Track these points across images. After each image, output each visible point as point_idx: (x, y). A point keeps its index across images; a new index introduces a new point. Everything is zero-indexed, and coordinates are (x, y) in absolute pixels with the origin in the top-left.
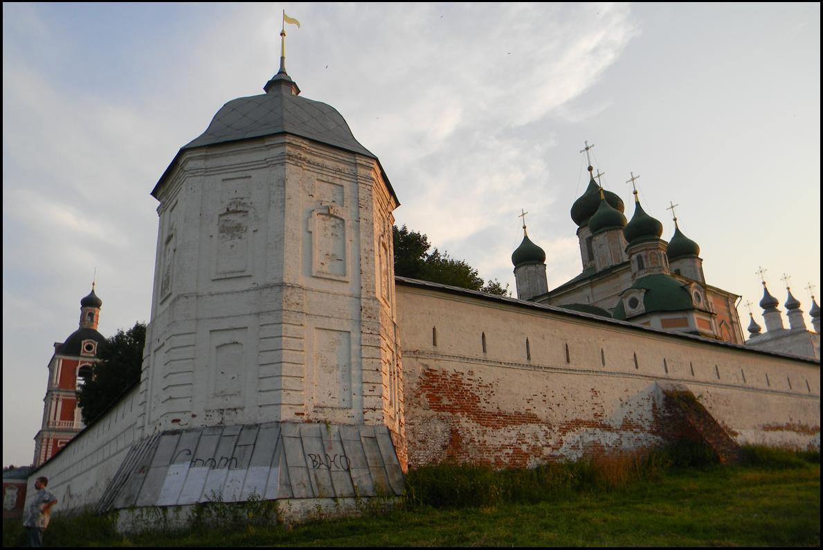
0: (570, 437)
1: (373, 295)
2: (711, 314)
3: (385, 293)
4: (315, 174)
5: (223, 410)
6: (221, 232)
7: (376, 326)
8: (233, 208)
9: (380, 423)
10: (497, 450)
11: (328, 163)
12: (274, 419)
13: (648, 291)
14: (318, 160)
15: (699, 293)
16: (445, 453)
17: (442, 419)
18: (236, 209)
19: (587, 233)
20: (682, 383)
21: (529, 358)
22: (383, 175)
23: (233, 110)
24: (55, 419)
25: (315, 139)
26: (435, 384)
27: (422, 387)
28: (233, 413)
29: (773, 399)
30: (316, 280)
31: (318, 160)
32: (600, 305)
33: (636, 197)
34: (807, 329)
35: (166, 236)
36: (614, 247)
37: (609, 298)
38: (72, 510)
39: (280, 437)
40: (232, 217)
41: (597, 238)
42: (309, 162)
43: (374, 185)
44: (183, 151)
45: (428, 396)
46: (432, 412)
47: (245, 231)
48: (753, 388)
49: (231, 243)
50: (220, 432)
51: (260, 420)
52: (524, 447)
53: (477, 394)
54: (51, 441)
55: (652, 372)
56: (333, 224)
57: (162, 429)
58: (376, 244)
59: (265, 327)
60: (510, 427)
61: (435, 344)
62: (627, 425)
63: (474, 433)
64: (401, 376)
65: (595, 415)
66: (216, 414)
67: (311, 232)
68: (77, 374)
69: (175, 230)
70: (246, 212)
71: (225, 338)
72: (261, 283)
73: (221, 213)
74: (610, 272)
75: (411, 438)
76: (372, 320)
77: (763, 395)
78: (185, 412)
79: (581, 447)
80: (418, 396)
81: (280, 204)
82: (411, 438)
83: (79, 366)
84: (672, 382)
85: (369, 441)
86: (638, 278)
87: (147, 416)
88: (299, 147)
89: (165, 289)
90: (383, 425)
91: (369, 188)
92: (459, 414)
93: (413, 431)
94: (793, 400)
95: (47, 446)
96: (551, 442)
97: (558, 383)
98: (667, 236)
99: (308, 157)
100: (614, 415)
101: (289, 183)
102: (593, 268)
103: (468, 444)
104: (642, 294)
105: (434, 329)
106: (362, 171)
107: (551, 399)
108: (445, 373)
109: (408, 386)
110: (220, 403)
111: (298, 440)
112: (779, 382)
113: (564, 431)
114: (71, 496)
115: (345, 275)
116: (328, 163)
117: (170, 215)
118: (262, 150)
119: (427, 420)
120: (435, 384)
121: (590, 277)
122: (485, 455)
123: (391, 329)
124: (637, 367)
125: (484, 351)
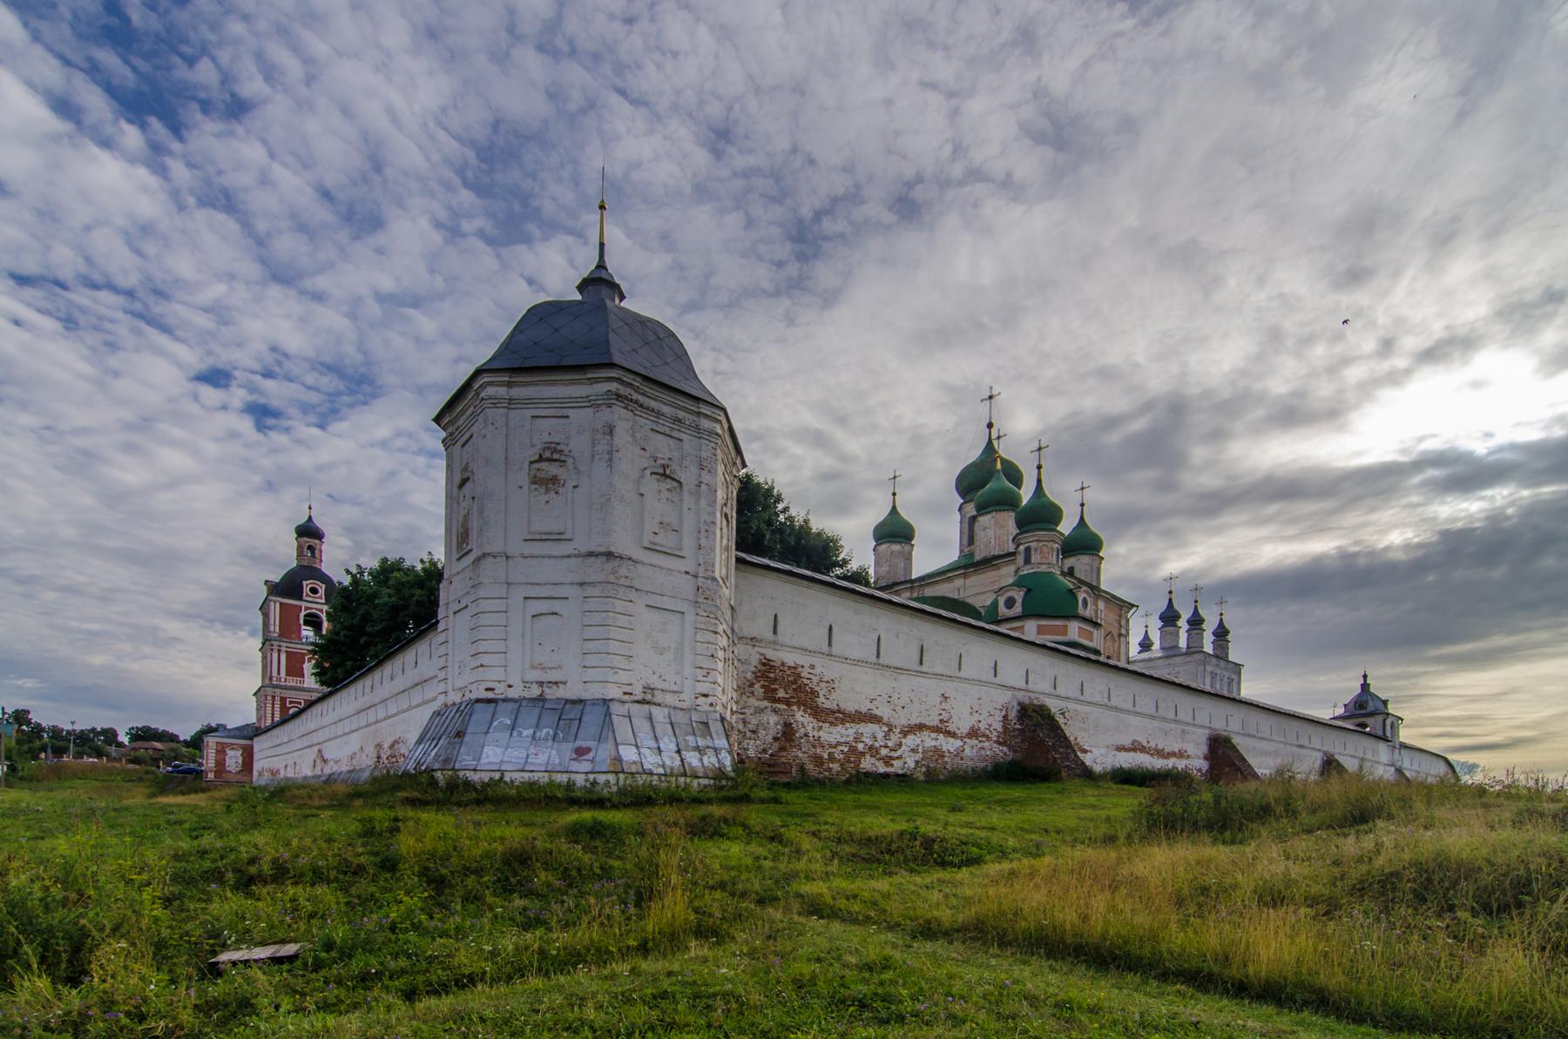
0: (911, 740)
1: (711, 574)
2: (1096, 625)
3: (724, 572)
4: (647, 422)
5: (543, 683)
6: (534, 483)
7: (714, 609)
8: (547, 454)
9: (712, 709)
10: (831, 746)
11: (666, 409)
12: (601, 696)
13: (1029, 590)
14: (653, 404)
15: (1088, 599)
16: (776, 745)
17: (775, 711)
18: (552, 454)
19: (971, 509)
20: (1041, 696)
21: (878, 656)
22: (731, 429)
23: (541, 319)
24: (279, 673)
25: (652, 376)
26: (772, 675)
27: (758, 677)
28: (555, 686)
29: (1134, 720)
30: (647, 552)
31: (653, 404)
32: (971, 601)
33: (1039, 474)
34: (1205, 650)
35: (458, 479)
36: (998, 530)
37: (984, 593)
38: (330, 775)
39: (608, 714)
40: (544, 465)
41: (981, 519)
42: (641, 406)
43: (719, 442)
44: (479, 372)
45: (763, 687)
46: (765, 703)
47: (563, 485)
48: (1116, 708)
49: (546, 498)
50: (541, 704)
51: (585, 696)
52: (860, 747)
53: (816, 689)
54: (278, 699)
55: (1011, 682)
56: (669, 486)
57: (474, 696)
58: (718, 515)
59: (590, 599)
60: (847, 725)
61: (775, 632)
62: (973, 733)
63: (809, 728)
64: (736, 664)
65: (941, 721)
66: (535, 686)
67: (642, 495)
68: (302, 622)
69: (472, 472)
70: (565, 461)
71: (543, 606)
72: (583, 550)
73: (533, 459)
74: (989, 562)
75: (741, 727)
76: (710, 602)
77: (1123, 715)
78: (500, 682)
79: (920, 750)
80: (752, 685)
81: (607, 457)
82: (741, 727)
83: (302, 615)
84: (1030, 694)
85: (700, 726)
86: (1021, 573)
87: (450, 681)
88: (630, 385)
89: (462, 544)
90: (715, 711)
91: (714, 445)
92: (795, 708)
93: (744, 722)
94: (1156, 723)
95: (273, 704)
96: (890, 744)
97: (907, 684)
98: (1066, 527)
99: (641, 399)
100: (962, 724)
101: (619, 431)
102: (972, 554)
103: (801, 738)
104: (1022, 594)
105: (776, 616)
106: (705, 424)
107: (896, 701)
108: (783, 664)
109: (741, 675)
110: (537, 675)
111: (628, 719)
112: (1145, 704)
113: (905, 734)
114: (325, 761)
115: (680, 550)
116: (666, 409)
117: (461, 452)
118: (581, 383)
119: (762, 711)
120: (772, 675)
121: (970, 565)
122: (819, 750)
123: (729, 612)
124: (995, 676)
125: (830, 645)
